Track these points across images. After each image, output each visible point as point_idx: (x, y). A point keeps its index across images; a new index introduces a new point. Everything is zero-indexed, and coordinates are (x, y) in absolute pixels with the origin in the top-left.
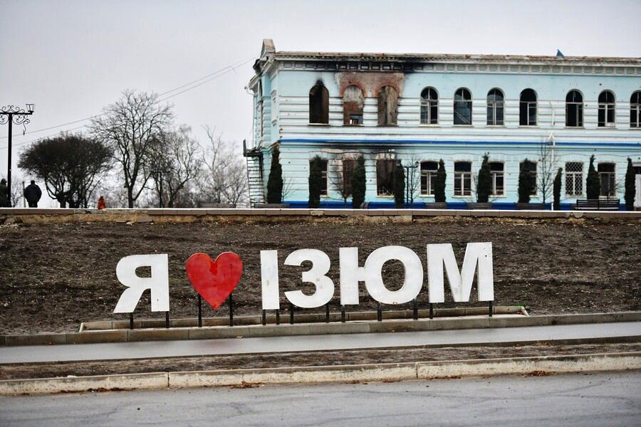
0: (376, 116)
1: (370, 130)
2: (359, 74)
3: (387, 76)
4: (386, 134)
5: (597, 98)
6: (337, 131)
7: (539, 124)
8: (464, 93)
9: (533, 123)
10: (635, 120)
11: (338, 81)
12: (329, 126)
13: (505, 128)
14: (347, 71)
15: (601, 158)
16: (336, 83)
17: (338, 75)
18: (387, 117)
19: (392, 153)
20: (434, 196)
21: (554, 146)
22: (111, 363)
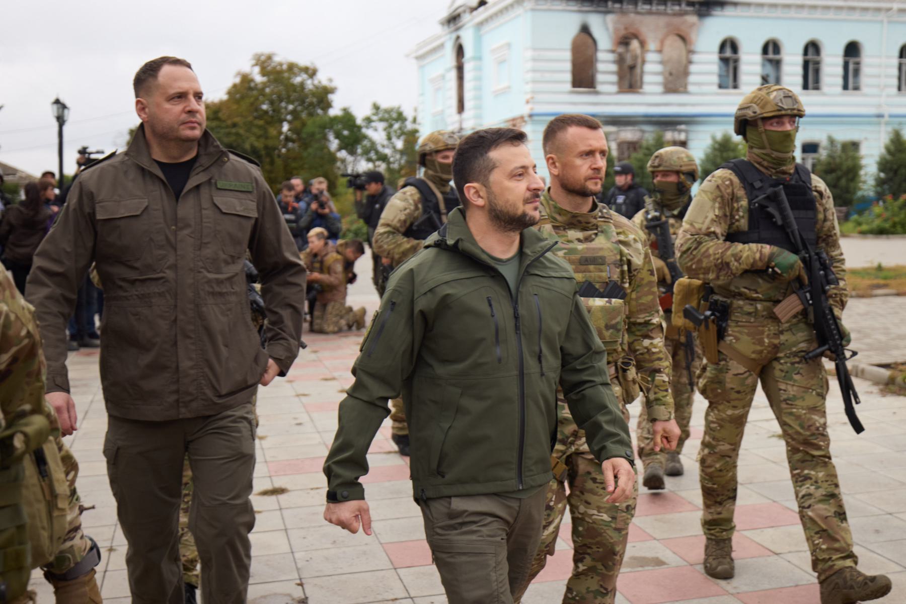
0: (614, 78)
1: (651, 99)
2: (638, 18)
3: (677, 20)
4: (673, 105)
5: (896, 53)
6: (608, 100)
7: (865, 89)
8: (812, 48)
9: (856, 88)
10: (904, 82)
11: (611, 26)
12: (597, 93)
13: (824, 94)
14: (623, 12)
15: (843, 135)
16: (607, 29)
17: (610, 18)
18: (676, 82)
19: (680, 131)
20: (71, 169)
21: (886, 119)
22: (356, 576)
